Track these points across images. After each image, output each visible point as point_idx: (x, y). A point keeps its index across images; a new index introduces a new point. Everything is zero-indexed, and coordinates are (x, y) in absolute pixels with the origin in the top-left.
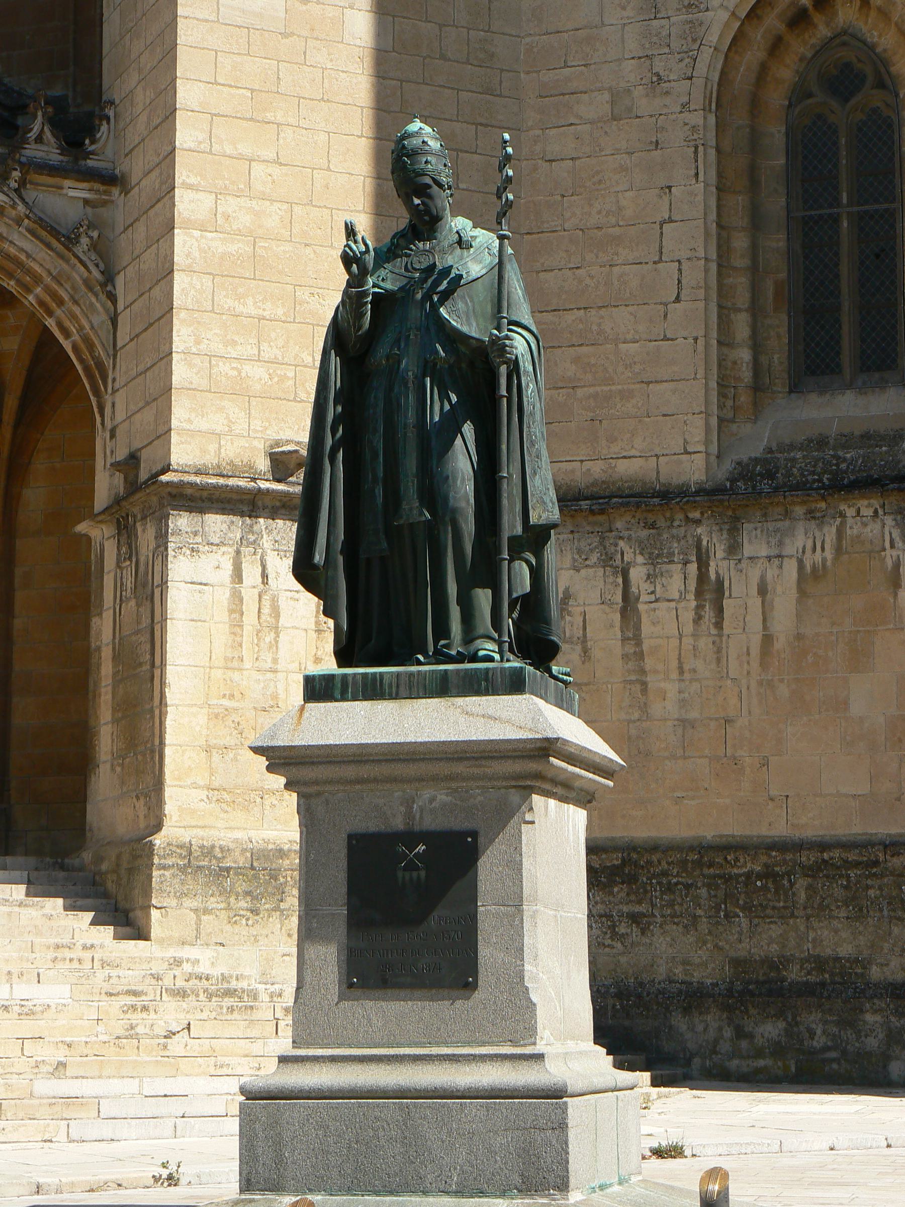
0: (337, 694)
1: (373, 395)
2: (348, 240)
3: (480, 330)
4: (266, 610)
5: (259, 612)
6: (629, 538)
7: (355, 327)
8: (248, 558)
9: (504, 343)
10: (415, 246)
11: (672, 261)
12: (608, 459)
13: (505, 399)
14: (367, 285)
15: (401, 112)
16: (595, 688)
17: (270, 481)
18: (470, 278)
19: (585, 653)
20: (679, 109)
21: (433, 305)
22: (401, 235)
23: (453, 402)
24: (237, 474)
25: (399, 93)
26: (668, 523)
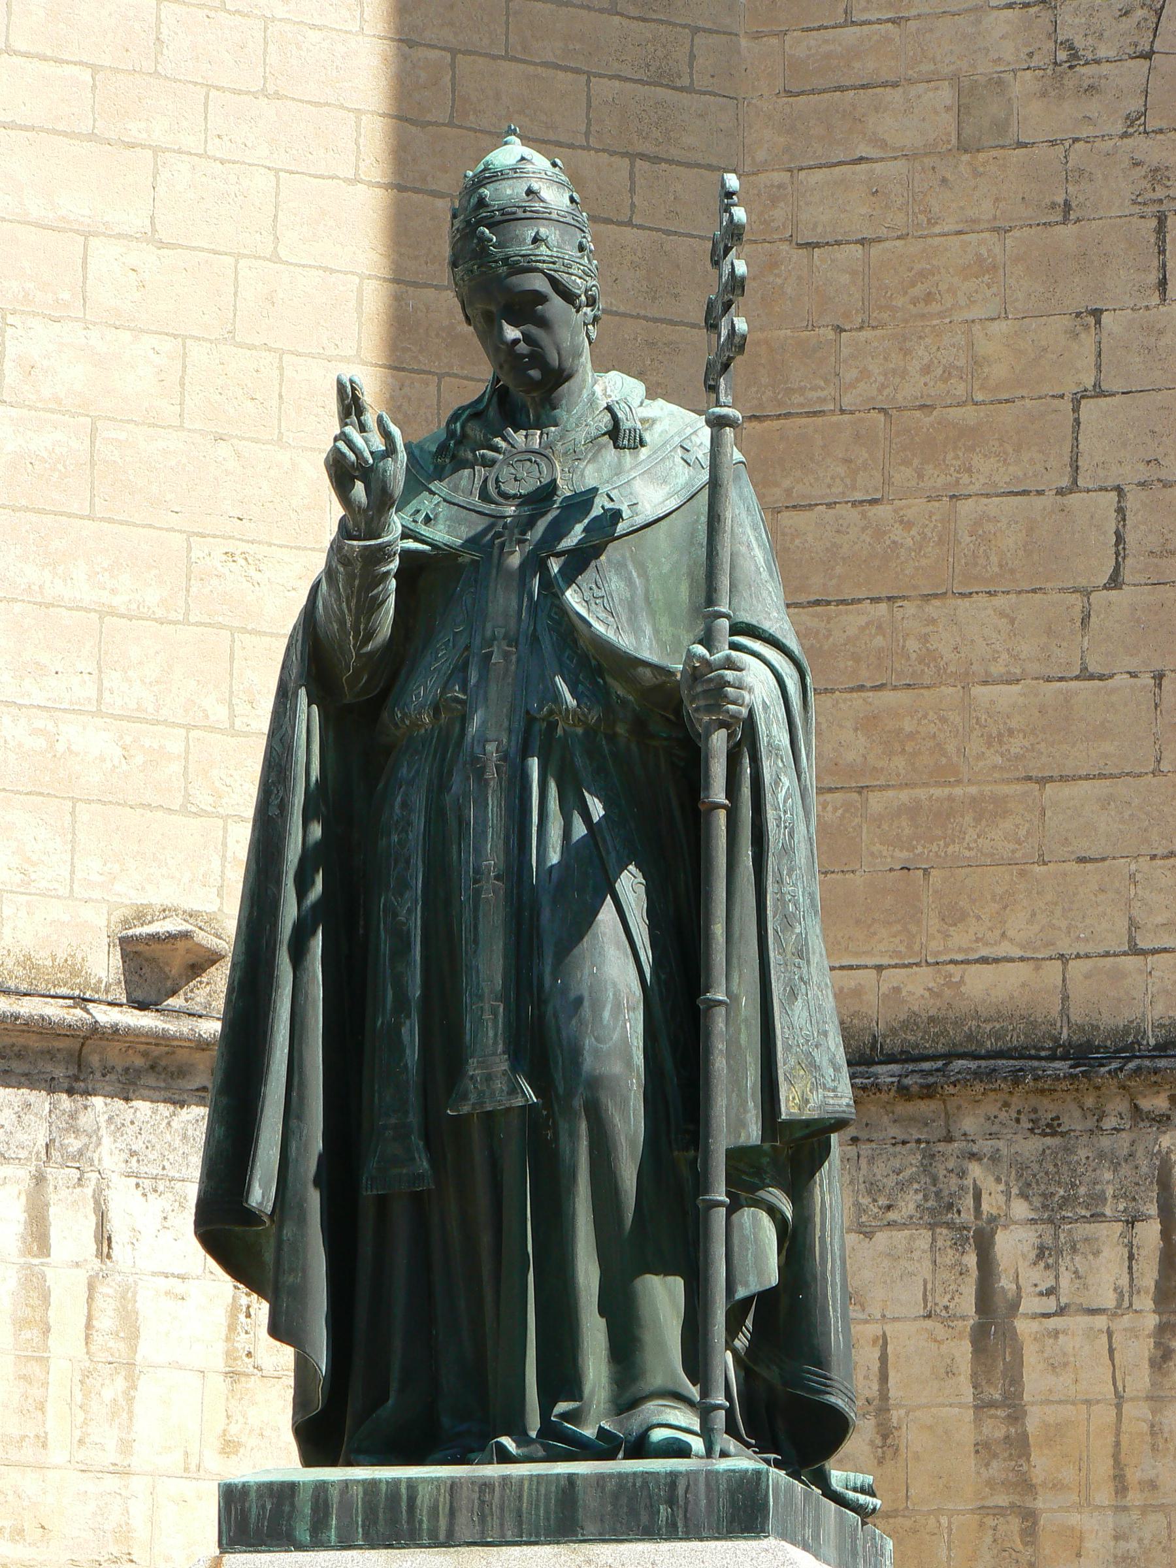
0: (303, 1532)
1: (399, 799)
2: (344, 424)
3: (662, 645)
4: (105, 1322)
5: (89, 1326)
6: (995, 1158)
7: (356, 637)
8: (64, 1193)
9: (721, 677)
10: (505, 439)
11: (1101, 489)
12: (945, 963)
13: (722, 815)
14: (389, 533)
15: (450, 124)
16: (908, 1523)
17: (121, 1005)
18: (640, 520)
19: (885, 1437)
20: (1120, 128)
21: (547, 584)
22: (475, 412)
23: (596, 819)
24: (42, 988)
25: (447, 79)
26: (1091, 1123)
